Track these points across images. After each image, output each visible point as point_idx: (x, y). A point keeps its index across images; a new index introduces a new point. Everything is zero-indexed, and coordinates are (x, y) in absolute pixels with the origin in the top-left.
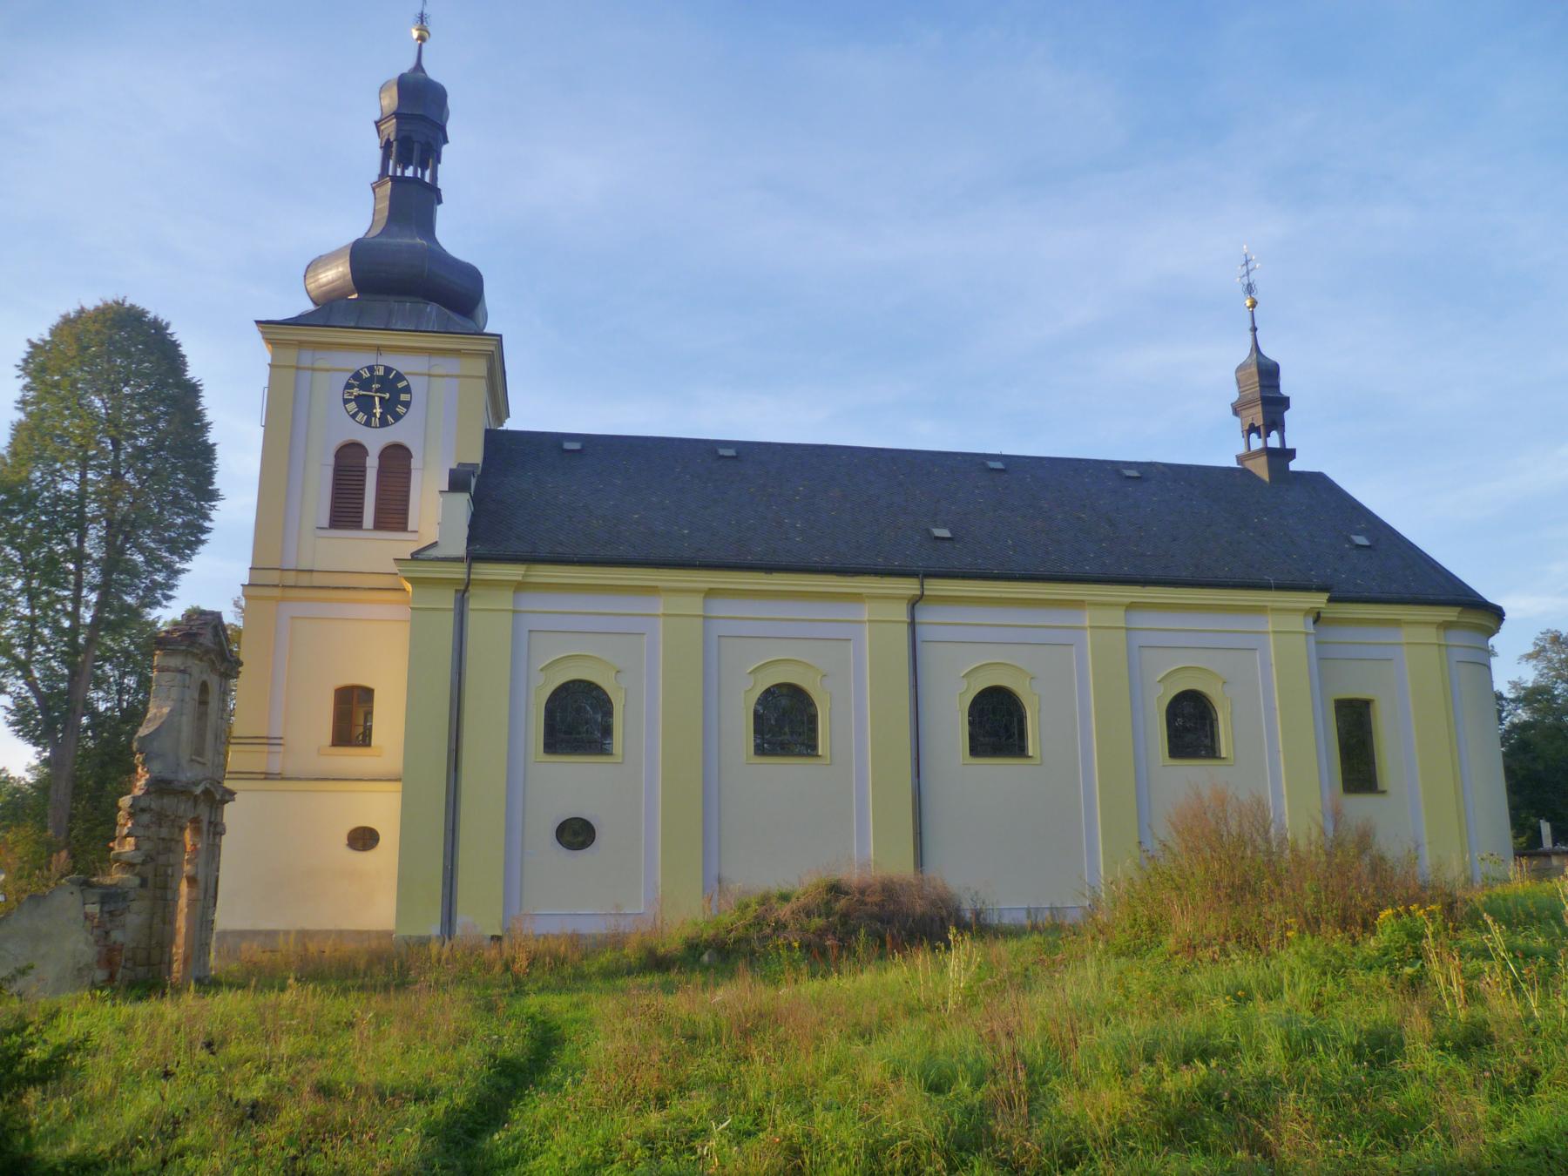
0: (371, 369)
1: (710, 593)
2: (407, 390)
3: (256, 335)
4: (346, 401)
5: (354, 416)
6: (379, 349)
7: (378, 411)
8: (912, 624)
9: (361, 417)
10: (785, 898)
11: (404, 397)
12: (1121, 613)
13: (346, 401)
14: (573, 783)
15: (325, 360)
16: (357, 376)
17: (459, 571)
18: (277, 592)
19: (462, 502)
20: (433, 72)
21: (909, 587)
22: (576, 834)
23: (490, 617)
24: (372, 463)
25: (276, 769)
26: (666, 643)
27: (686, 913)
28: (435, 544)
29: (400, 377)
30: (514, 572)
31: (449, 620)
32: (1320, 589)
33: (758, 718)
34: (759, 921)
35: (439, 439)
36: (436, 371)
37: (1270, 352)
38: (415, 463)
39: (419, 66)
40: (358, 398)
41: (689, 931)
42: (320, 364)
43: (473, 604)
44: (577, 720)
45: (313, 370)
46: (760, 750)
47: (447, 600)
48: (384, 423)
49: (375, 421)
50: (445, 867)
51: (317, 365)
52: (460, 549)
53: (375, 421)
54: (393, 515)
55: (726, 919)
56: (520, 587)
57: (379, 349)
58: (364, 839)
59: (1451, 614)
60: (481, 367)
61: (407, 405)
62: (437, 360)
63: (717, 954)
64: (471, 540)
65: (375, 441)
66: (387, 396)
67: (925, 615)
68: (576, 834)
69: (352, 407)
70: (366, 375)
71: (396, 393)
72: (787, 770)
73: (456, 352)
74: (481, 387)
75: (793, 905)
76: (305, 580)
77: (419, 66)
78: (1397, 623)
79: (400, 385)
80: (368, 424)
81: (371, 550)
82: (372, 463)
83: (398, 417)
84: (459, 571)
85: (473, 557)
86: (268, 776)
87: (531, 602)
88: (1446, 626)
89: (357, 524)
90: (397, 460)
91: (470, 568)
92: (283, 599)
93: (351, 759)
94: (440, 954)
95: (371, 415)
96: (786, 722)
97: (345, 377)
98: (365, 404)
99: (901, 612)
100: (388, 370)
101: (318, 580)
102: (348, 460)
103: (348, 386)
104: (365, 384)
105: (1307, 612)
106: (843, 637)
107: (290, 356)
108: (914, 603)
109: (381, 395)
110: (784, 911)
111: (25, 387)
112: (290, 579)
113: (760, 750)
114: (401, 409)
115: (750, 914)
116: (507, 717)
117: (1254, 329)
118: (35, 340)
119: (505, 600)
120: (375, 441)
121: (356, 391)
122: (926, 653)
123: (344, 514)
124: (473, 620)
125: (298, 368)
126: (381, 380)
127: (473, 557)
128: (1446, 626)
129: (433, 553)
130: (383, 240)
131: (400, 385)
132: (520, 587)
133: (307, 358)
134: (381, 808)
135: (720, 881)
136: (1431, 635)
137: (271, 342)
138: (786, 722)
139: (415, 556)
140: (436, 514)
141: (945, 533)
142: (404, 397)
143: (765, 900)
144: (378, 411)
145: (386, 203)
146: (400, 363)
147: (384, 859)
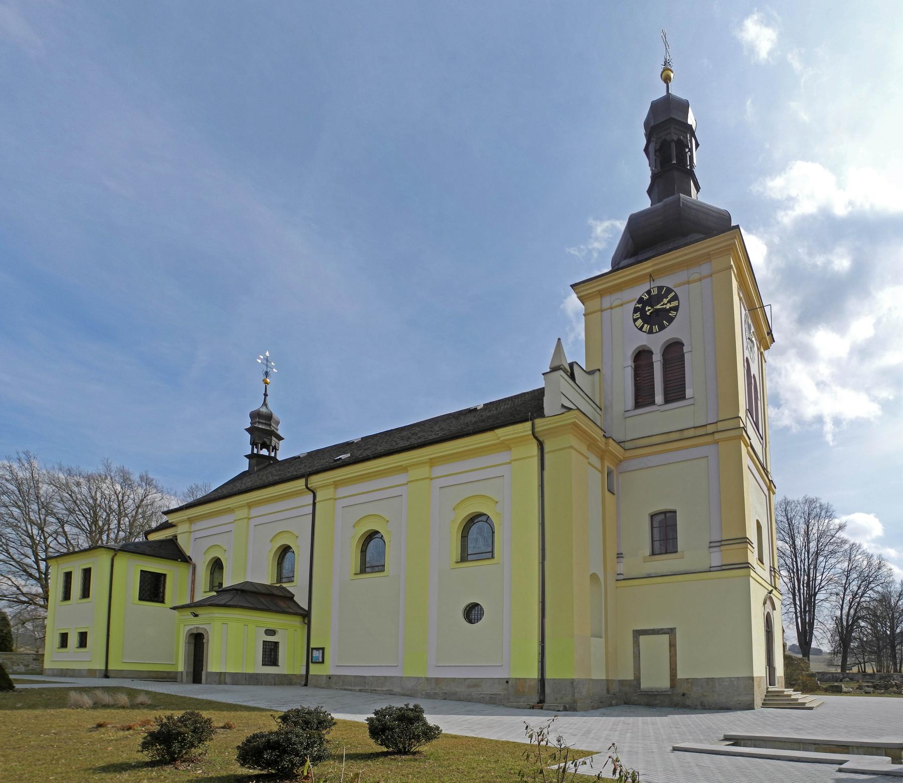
0: (649, 292)
29: (669, 290)
37: (273, 408)
65: (656, 342)
69: (639, 322)
100: (660, 288)
102: (642, 357)
117: (266, 395)
123: (643, 396)
146: (666, 282)
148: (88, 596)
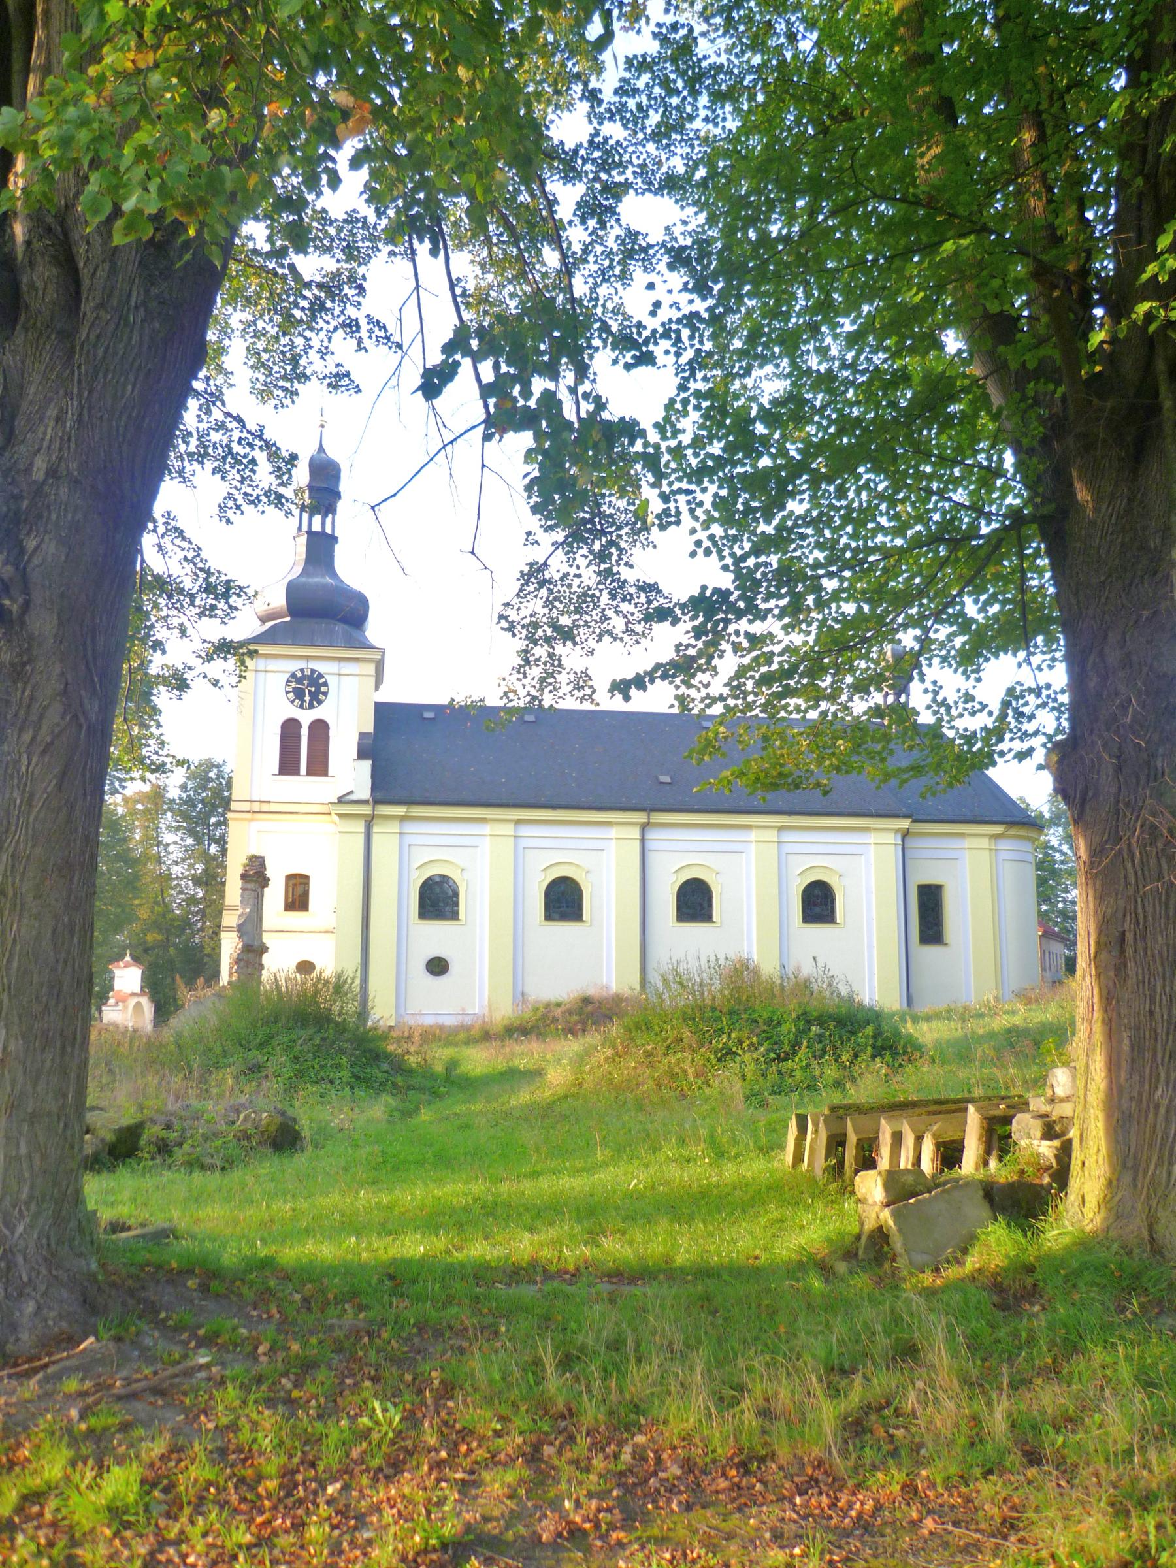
0: (302, 670)
1: (518, 822)
2: (325, 684)
6: (308, 658)
7: (307, 698)
8: (643, 841)
10: (558, 1005)
11: (323, 689)
12: (775, 832)
14: (435, 937)
15: (274, 665)
16: (293, 675)
17: (366, 810)
18: (248, 816)
19: (367, 765)
20: (333, 453)
21: (641, 817)
22: (438, 967)
23: (385, 839)
24: (305, 732)
26: (492, 854)
27: (504, 1011)
29: (321, 676)
30: (400, 810)
31: (361, 839)
32: (906, 816)
33: (547, 895)
34: (544, 1017)
35: (347, 714)
36: (343, 671)
39: (321, 449)
41: (506, 1022)
42: (269, 668)
43: (375, 829)
44: (438, 900)
46: (548, 917)
47: (360, 827)
48: (311, 706)
49: (306, 705)
52: (365, 793)
53: (306, 705)
54: (319, 767)
55: (526, 1016)
56: (403, 819)
57: (308, 658)
59: (999, 829)
60: (371, 669)
61: (325, 694)
62: (343, 664)
63: (519, 1030)
64: (374, 788)
65: (306, 717)
67: (651, 835)
68: (438, 967)
69: (291, 695)
70: (299, 674)
72: (564, 930)
73: (357, 660)
75: (563, 1008)
76: (265, 807)
77: (321, 449)
78: (963, 835)
80: (301, 707)
81: (303, 786)
82: (305, 732)
83: (320, 702)
84: (366, 810)
85: (376, 801)
87: (410, 828)
88: (997, 837)
89: (295, 771)
90: (320, 729)
95: (303, 701)
96: (564, 901)
98: (299, 694)
99: (635, 833)
100: (313, 671)
101: (273, 807)
102: (290, 729)
104: (299, 681)
105: (897, 831)
106: (602, 852)
108: (644, 827)
109: (309, 689)
110: (558, 1012)
112: (256, 807)
113: (548, 917)
114: (321, 697)
115: (539, 1013)
116: (395, 897)
119: (395, 827)
120: (306, 717)
122: (652, 858)
123: (288, 766)
124: (375, 838)
126: (310, 678)
127: (376, 801)
128: (997, 837)
129: (352, 797)
130: (303, 579)
132: (403, 819)
135: (1135, 1186)
136: (985, 843)
138: (564, 901)
139: (340, 800)
140: (350, 773)
141: (667, 779)
143: (548, 1005)
145: (304, 549)
148: (307, 877)
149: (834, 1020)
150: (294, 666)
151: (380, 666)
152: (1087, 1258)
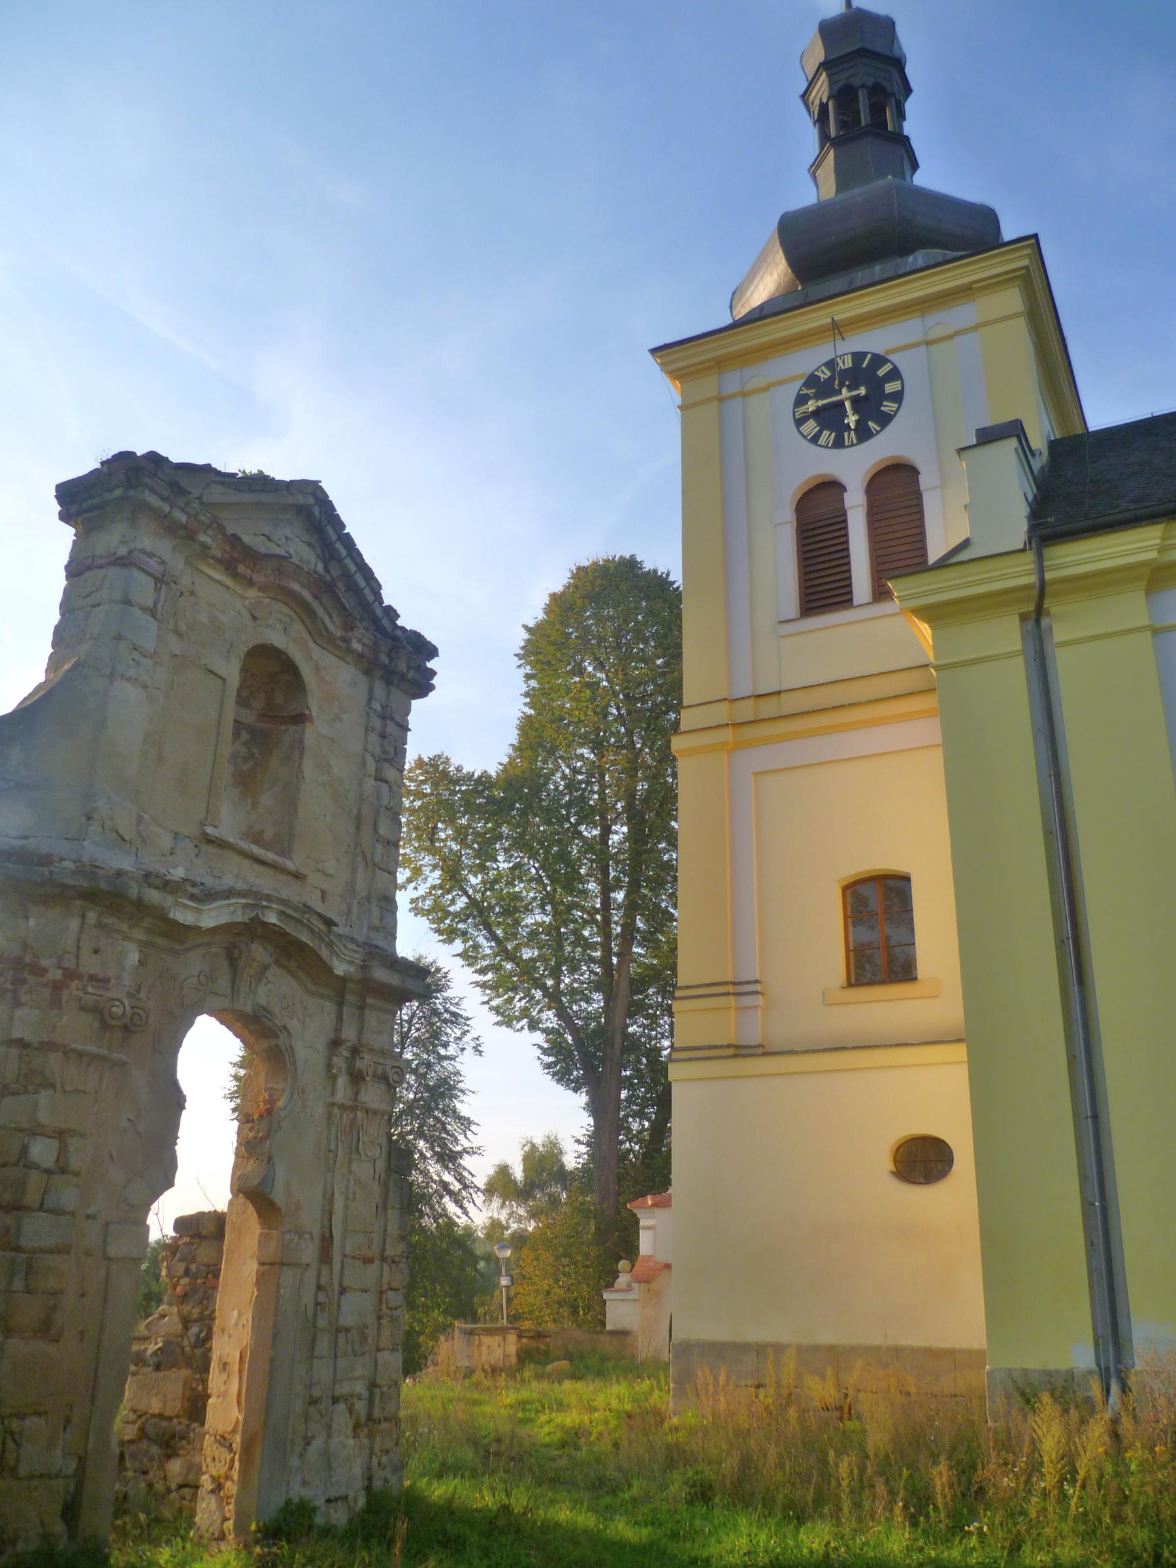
0: (831, 364)
2: (895, 374)
3: (652, 365)
4: (799, 422)
5: (815, 440)
6: (837, 329)
7: (852, 419)
9: (827, 436)
11: (891, 387)
13: (799, 422)
25: (753, 1037)
28: (965, 544)
29: (879, 360)
31: (1015, 677)
36: (935, 334)
38: (924, 482)
40: (816, 414)
43: (1060, 632)
45: (744, 394)
47: (1005, 635)
48: (864, 434)
50: (1086, 1204)
51: (749, 387)
58: (922, 1160)
60: (1012, 300)
61: (898, 397)
65: (853, 466)
66: (862, 391)
69: (811, 426)
71: (876, 385)
74: (1019, 335)
76: (769, 708)
79: (881, 372)
80: (839, 444)
83: (885, 420)
84: (1021, 573)
86: (740, 1051)
90: (896, 487)
91: (1040, 558)
92: (738, 746)
93: (885, 1007)
94: (1069, 1459)
97: (794, 388)
98: (830, 417)
100: (858, 357)
101: (790, 704)
102: (817, 520)
103: (801, 400)
107: (707, 386)
109: (857, 397)
111: (528, 677)
114: (888, 407)
118: (531, 624)
119: (1132, 608)
121: (811, 406)
124: (1067, 665)
125: (721, 399)
131: (881, 372)
133: (733, 381)
134: (936, 1095)
137: (676, 374)
142: (891, 387)
144: (852, 419)
146: (871, 342)
147: (955, 1198)
148: (906, 879)
149: (55, 1306)
150: (811, 360)
151: (1036, 286)
152: (276, 1010)
